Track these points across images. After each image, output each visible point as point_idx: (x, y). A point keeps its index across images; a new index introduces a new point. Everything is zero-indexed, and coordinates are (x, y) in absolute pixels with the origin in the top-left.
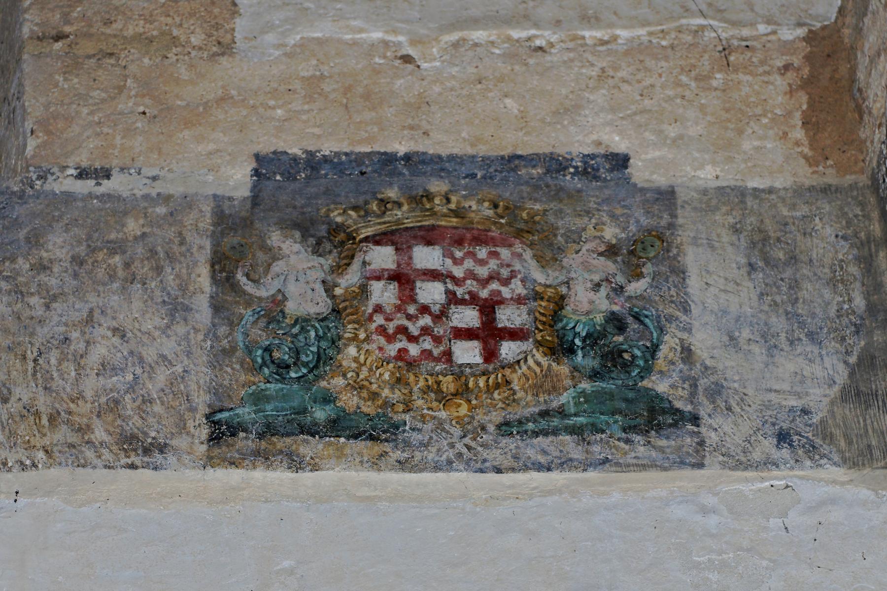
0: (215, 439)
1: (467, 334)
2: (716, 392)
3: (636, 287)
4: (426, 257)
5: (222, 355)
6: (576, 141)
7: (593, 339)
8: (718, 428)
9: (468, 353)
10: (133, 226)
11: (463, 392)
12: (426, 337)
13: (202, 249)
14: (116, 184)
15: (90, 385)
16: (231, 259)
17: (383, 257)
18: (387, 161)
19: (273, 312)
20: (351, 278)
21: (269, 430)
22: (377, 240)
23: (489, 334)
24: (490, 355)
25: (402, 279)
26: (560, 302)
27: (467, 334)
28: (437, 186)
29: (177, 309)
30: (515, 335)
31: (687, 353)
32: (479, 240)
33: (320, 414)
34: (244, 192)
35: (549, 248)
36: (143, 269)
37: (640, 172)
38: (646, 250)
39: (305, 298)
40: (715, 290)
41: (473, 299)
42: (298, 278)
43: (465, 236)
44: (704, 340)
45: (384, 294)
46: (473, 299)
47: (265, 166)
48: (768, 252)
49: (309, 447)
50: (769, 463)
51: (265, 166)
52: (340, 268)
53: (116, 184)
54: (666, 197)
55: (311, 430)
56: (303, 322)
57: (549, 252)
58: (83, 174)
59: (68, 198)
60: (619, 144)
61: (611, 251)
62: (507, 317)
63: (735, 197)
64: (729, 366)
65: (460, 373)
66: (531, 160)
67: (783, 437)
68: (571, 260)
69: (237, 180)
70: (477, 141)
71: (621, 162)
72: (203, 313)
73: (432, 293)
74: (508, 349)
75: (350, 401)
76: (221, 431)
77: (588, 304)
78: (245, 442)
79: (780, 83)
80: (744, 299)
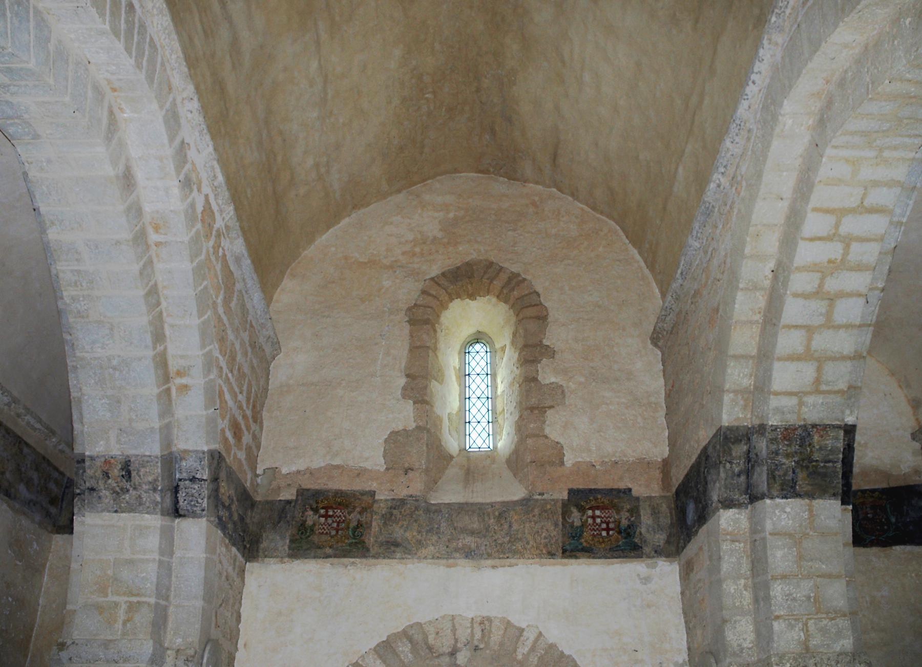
0: (563, 553)
1: (604, 529)
2: (645, 541)
3: (633, 519)
4: (598, 513)
5: (564, 535)
6: (622, 485)
7: (625, 530)
8: (647, 550)
9: (604, 533)
10: (548, 507)
11: (603, 542)
12: (478, 347)
13: (560, 511)
14: (545, 496)
15: (543, 541)
16: (565, 513)
17: (590, 513)
18: (591, 490)
19: (572, 526)
20: (585, 518)
21: (572, 551)
22: (589, 509)
23: (608, 530)
24: (608, 534)
25: (594, 517)
26: (620, 522)
27: (604, 529)
28: (599, 497)
29: (556, 525)
30: (612, 529)
31: (641, 534)
32: (607, 509)
33: (580, 547)
34: (566, 498)
35: (618, 512)
36: (551, 516)
37: (634, 493)
38: (634, 512)
39: (577, 523)
40: (646, 519)
41: (605, 522)
42: (576, 517)
43: (602, 508)
44: (643, 530)
45: (590, 521)
46: (605, 522)
47: (571, 492)
48: (655, 512)
49: (579, 554)
50: (654, 557)
51: (571, 492)
52: (583, 515)
53: (545, 496)
54: (637, 499)
55: (578, 551)
56: (577, 527)
57: (618, 512)
58: (540, 494)
59: (537, 500)
60: (630, 486)
61: (628, 511)
62: (611, 526)
63: (650, 498)
64: (648, 537)
65: (603, 537)
66: (615, 490)
67: (656, 552)
68: (622, 513)
69: (565, 495)
70: (654, 566)
71: (630, 490)
72: (561, 526)
73: (598, 520)
74: (611, 533)
75: (585, 544)
76: (564, 551)
77: (624, 523)
78: (568, 553)
79: (658, 471)
80: (650, 522)
